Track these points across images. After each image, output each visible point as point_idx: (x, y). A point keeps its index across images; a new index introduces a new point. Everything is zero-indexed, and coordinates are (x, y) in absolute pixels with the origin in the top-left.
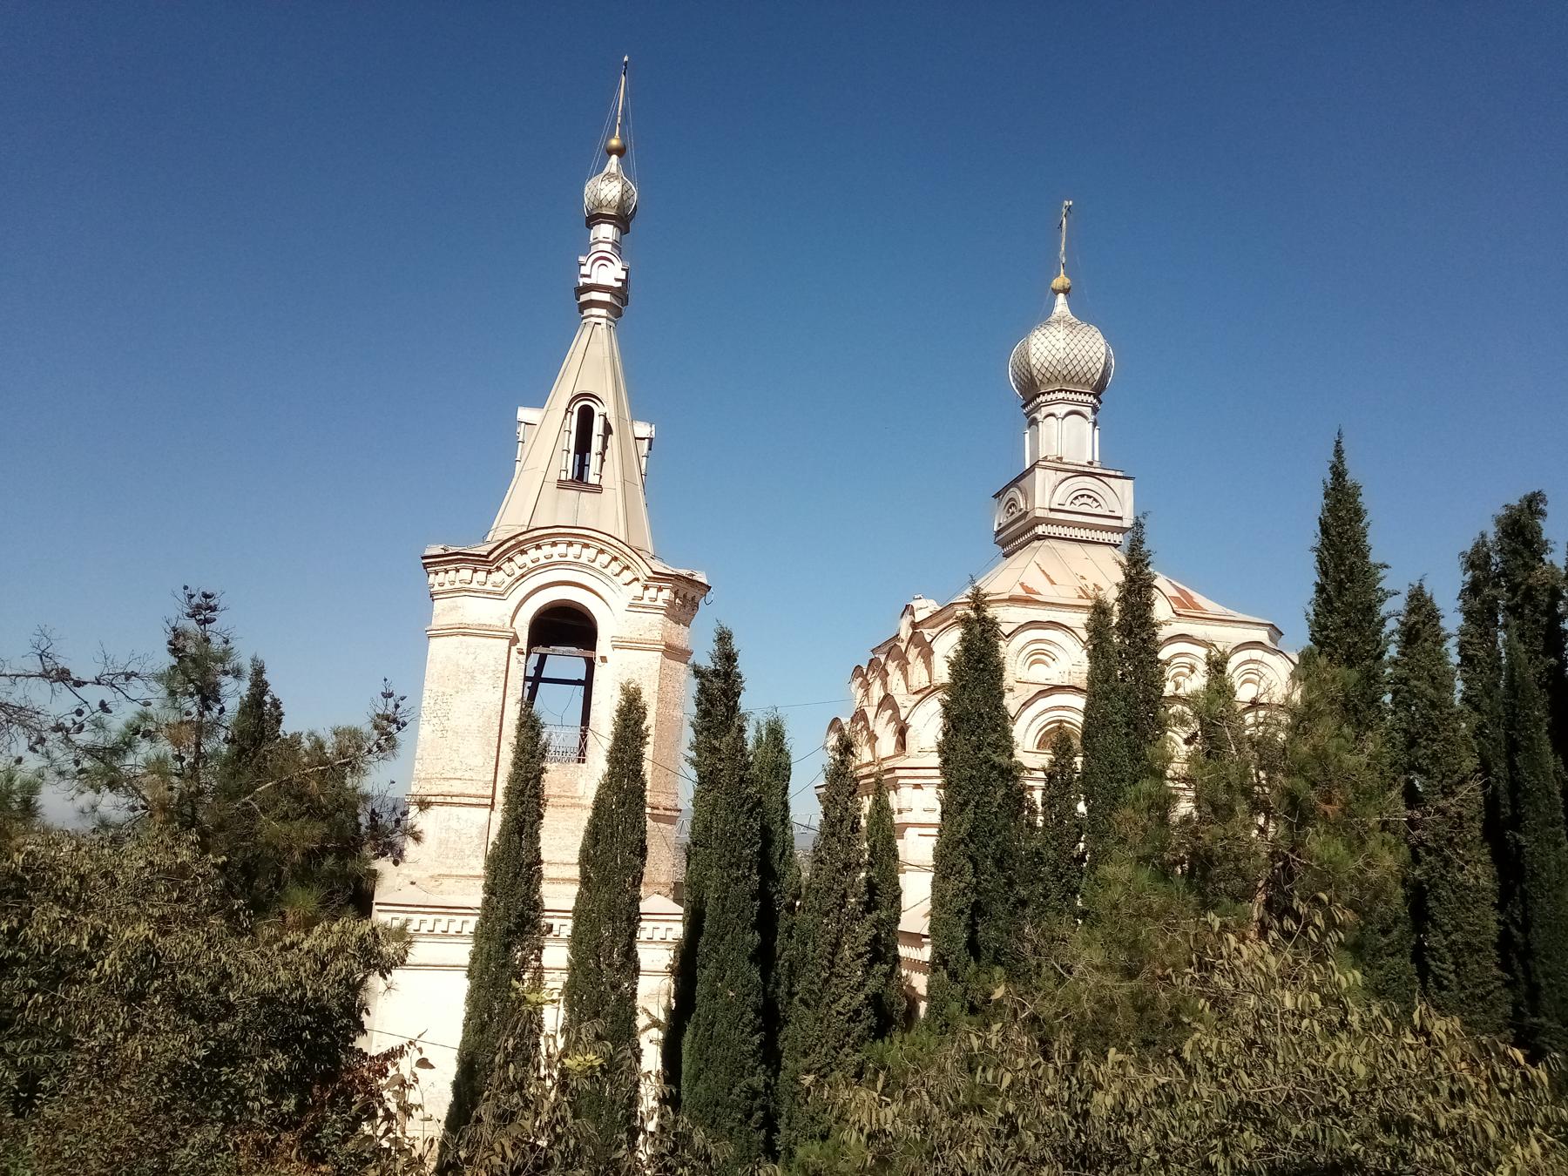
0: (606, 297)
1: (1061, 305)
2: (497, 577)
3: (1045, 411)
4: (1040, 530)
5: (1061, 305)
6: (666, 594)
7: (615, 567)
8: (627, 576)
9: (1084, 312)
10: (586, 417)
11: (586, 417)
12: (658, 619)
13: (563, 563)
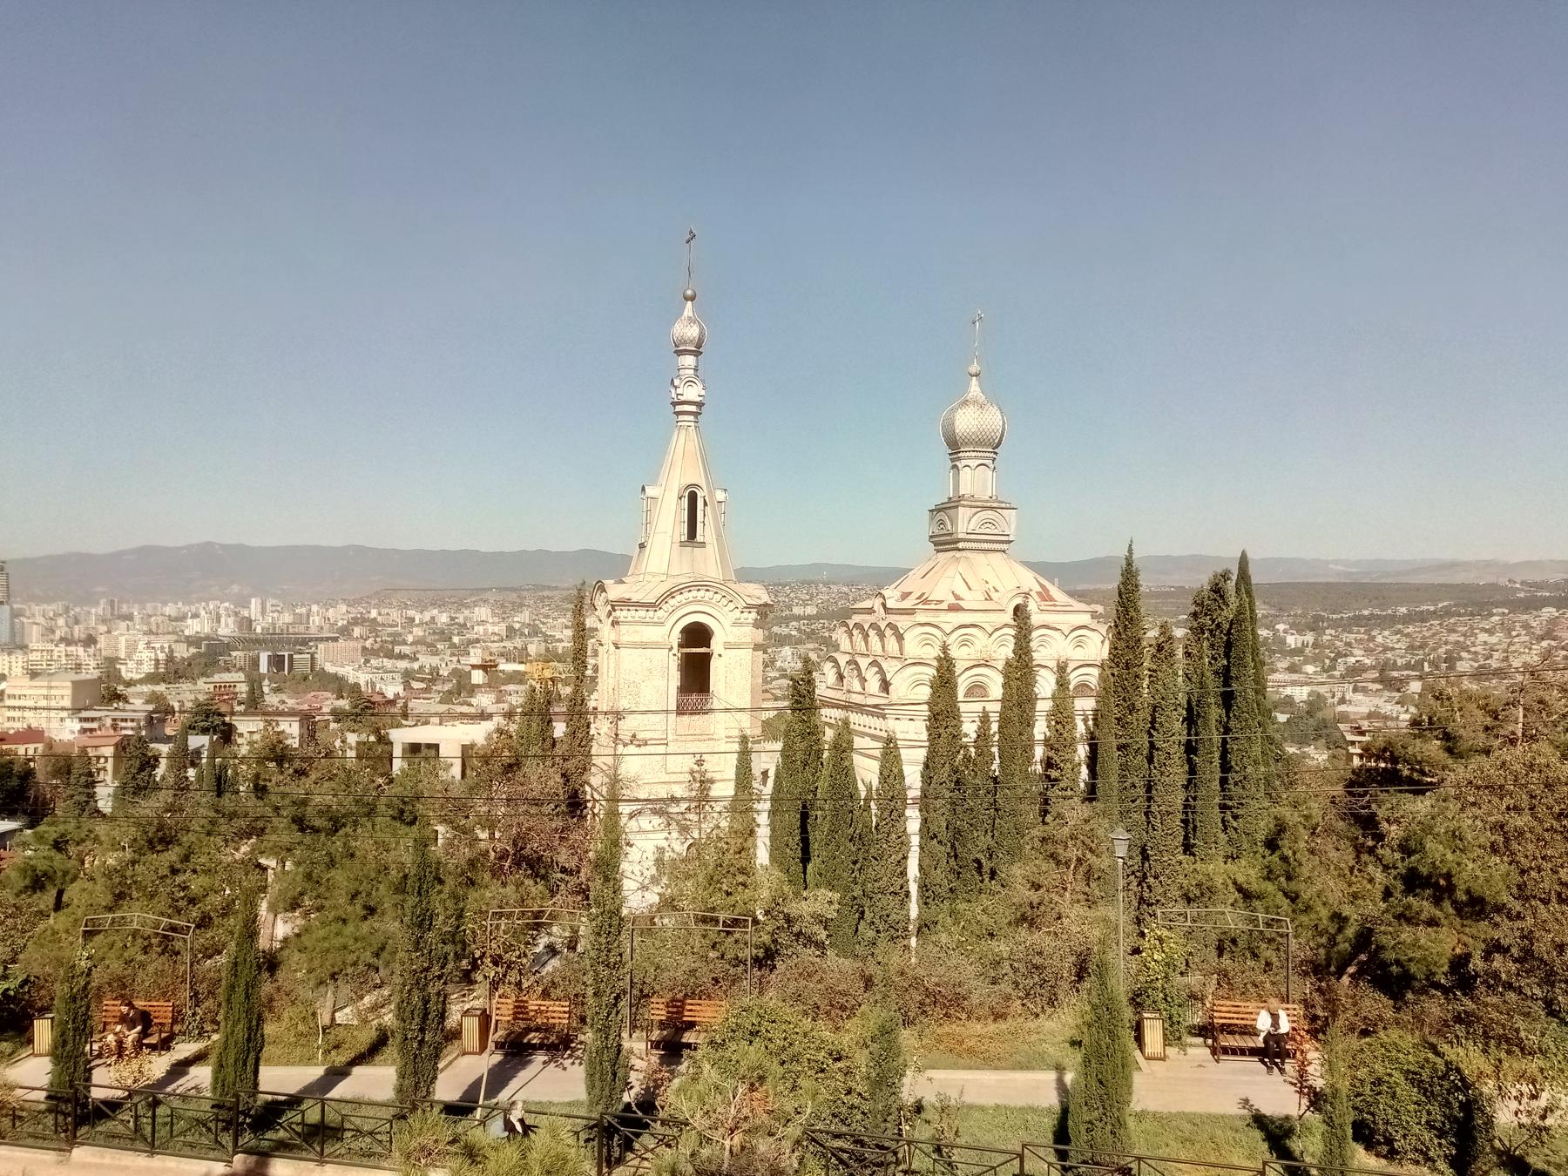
0: (693, 408)
1: (974, 388)
2: (660, 613)
3: (964, 462)
4: (960, 545)
5: (974, 388)
6: (754, 615)
7: (724, 601)
8: (731, 606)
9: (993, 397)
10: (693, 498)
11: (693, 498)
12: (749, 629)
13: (696, 601)
